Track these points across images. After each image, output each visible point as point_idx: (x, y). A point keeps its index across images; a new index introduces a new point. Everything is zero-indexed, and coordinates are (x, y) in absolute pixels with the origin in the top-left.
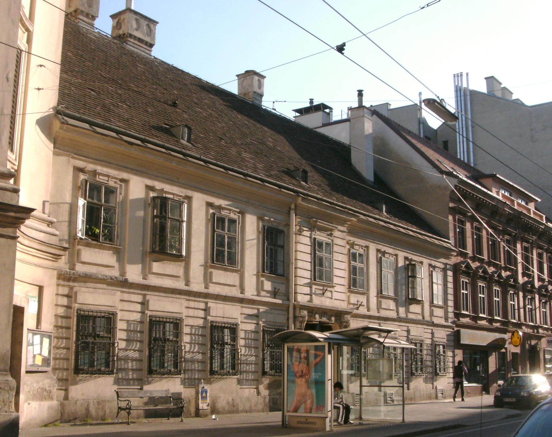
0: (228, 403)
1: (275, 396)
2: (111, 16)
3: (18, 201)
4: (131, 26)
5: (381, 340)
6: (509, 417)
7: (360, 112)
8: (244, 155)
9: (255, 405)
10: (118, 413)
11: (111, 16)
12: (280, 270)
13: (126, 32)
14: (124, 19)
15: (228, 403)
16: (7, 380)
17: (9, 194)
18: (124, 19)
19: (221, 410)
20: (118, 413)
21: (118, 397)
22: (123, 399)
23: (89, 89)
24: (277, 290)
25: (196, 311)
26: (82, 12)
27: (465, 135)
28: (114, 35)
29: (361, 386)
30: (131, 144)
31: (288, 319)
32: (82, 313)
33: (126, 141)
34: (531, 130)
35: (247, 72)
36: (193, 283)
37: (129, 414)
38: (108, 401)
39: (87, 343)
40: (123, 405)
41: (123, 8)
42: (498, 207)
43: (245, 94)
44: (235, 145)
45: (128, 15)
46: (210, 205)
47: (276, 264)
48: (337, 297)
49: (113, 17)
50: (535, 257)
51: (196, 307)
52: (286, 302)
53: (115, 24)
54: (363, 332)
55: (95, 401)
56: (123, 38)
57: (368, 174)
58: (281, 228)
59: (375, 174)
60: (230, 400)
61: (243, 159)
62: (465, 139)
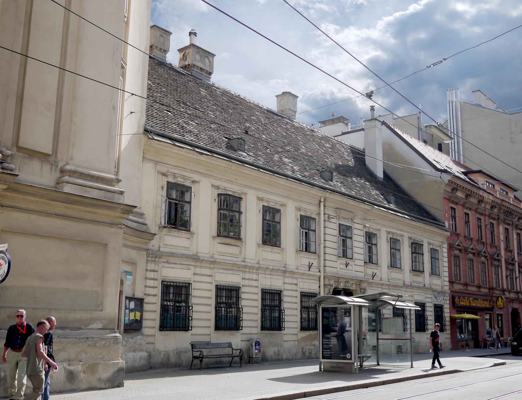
0: (275, 352)
1: (310, 347)
2: (178, 50)
3: (124, 201)
4: (193, 59)
5: (393, 303)
6: (496, 365)
7: (373, 123)
8: (286, 160)
9: (296, 355)
10: (193, 361)
11: (178, 50)
12: (312, 249)
13: (190, 63)
14: (189, 53)
15: (275, 352)
16: (116, 336)
17: (117, 195)
18: (189, 53)
19: (270, 358)
20: (193, 361)
21: (192, 348)
22: (196, 350)
23: (167, 111)
24: (311, 264)
25: (250, 281)
26: (157, 47)
27: (456, 150)
28: (181, 65)
29: (378, 339)
30: (202, 154)
31: (319, 287)
32: (165, 283)
33: (197, 152)
34: (511, 133)
35: (283, 93)
36: (145, 327)
37: (201, 361)
38: (185, 352)
39: (177, 310)
40: (197, 354)
41: (188, 44)
42: (483, 197)
43: (282, 111)
44: (278, 152)
45: (191, 51)
46: (260, 199)
47: (310, 244)
48: (357, 269)
49: (180, 50)
50: (515, 236)
51: (250, 278)
52: (319, 274)
53: (182, 57)
54: (380, 297)
55: (175, 352)
56: (188, 68)
57: (380, 174)
58: (313, 216)
59: (384, 172)
60: (276, 350)
61: (284, 164)
62: (456, 154)
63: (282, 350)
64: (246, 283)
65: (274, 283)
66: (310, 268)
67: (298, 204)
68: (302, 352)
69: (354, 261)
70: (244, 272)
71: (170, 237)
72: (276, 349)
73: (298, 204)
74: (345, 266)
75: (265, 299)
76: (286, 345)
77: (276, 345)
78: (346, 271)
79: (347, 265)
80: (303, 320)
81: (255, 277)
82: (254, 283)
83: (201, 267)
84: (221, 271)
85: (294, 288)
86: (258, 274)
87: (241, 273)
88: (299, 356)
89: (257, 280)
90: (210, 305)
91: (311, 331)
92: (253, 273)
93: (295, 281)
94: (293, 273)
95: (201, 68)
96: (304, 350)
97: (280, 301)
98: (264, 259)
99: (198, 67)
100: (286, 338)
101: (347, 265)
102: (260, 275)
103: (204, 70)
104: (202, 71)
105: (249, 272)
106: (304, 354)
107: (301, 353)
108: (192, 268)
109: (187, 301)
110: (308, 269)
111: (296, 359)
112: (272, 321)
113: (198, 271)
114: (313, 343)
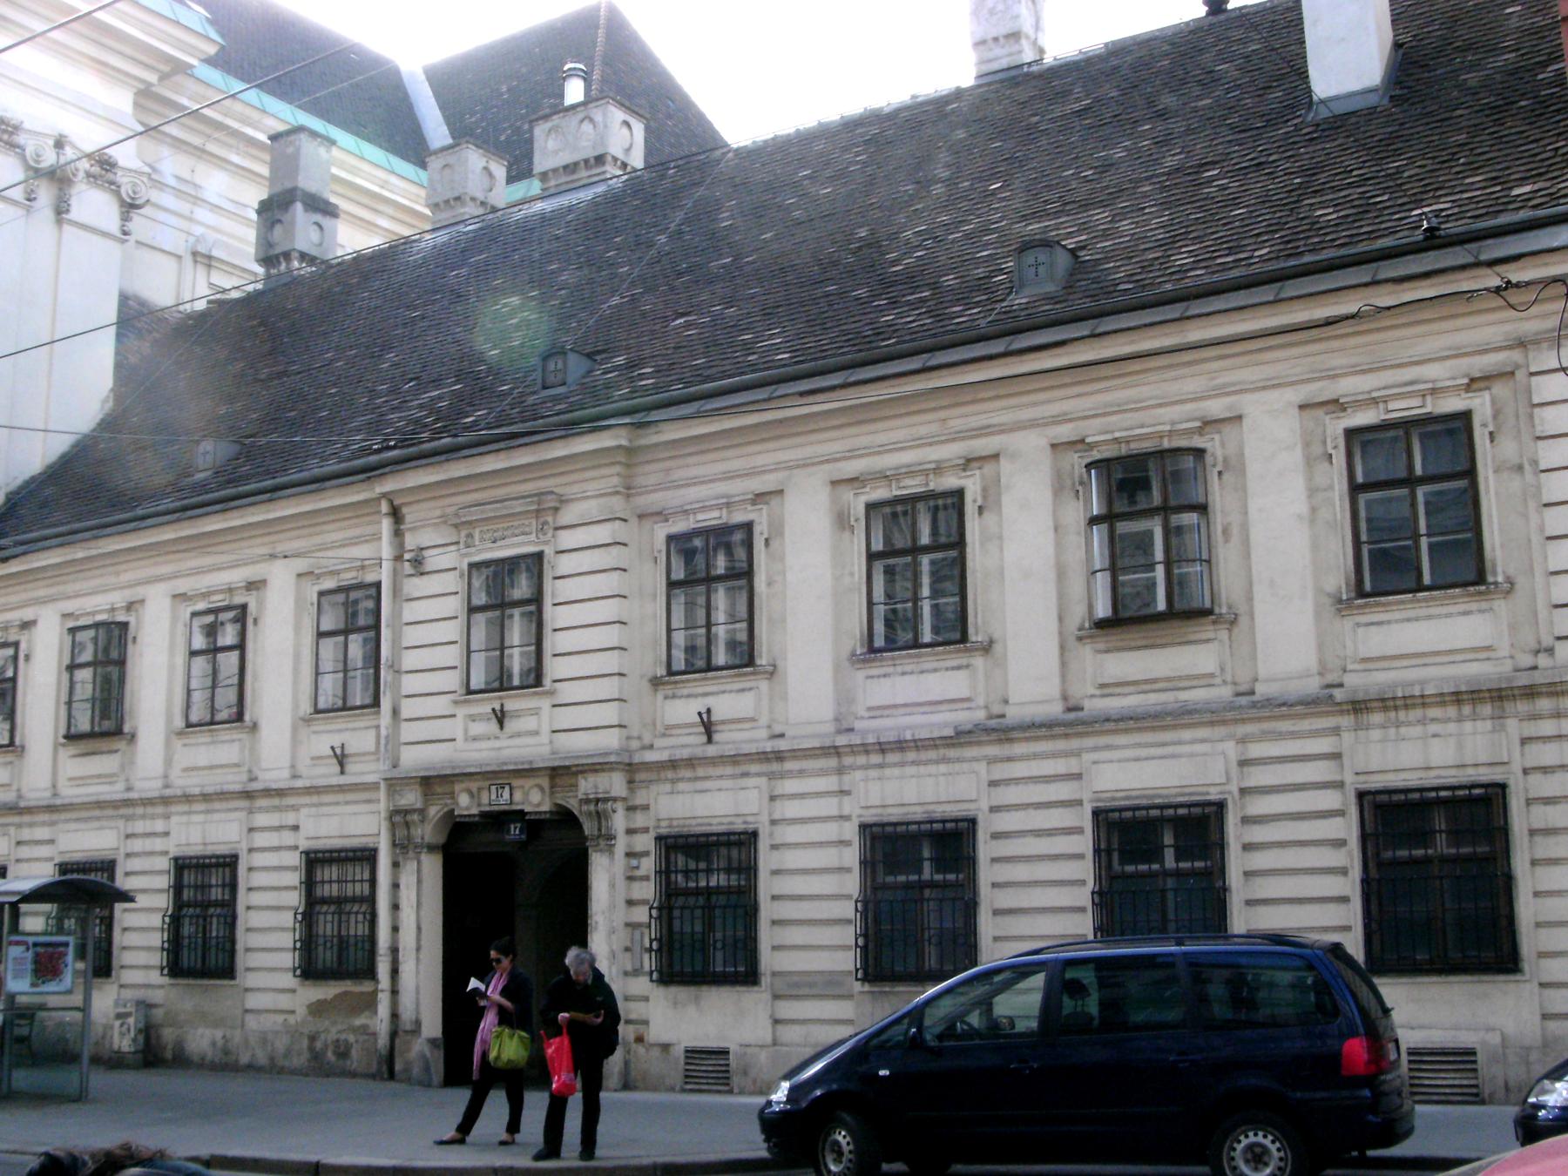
0: (214, 1044)
9: (288, 1053)
15: (214, 1044)
19: (196, 1059)
24: (338, 751)
63: (237, 1036)
64: (137, 845)
65: (210, 833)
66: (341, 764)
67: (301, 565)
68: (311, 1049)
69: (552, 693)
70: (128, 818)
71: (678, 702)
72: (219, 1034)
73: (301, 565)
74: (493, 726)
75: (224, 886)
76: (252, 1023)
77: (218, 1023)
78: (497, 744)
79: (501, 717)
80: (228, 946)
81: (159, 826)
82: (158, 844)
83: (31, 825)
84: (73, 826)
85: (288, 838)
86: (167, 817)
87: (121, 823)
88: (300, 1060)
89: (167, 834)
90: (997, 912)
91: (349, 982)
92: (153, 817)
93: (290, 818)
94: (280, 793)
95: (565, 167)
96: (319, 1045)
97: (233, 886)
98: (1102, 686)
99: (555, 170)
100: (253, 1001)
101: (501, 717)
102: (174, 819)
103: (576, 164)
104: (573, 172)
105: (143, 817)
106: (316, 1056)
107: (306, 1055)
108: (12, 830)
109: (179, 904)
110: (338, 769)
111: (282, 1071)
112: (336, 948)
113: (26, 834)
114: (358, 1022)
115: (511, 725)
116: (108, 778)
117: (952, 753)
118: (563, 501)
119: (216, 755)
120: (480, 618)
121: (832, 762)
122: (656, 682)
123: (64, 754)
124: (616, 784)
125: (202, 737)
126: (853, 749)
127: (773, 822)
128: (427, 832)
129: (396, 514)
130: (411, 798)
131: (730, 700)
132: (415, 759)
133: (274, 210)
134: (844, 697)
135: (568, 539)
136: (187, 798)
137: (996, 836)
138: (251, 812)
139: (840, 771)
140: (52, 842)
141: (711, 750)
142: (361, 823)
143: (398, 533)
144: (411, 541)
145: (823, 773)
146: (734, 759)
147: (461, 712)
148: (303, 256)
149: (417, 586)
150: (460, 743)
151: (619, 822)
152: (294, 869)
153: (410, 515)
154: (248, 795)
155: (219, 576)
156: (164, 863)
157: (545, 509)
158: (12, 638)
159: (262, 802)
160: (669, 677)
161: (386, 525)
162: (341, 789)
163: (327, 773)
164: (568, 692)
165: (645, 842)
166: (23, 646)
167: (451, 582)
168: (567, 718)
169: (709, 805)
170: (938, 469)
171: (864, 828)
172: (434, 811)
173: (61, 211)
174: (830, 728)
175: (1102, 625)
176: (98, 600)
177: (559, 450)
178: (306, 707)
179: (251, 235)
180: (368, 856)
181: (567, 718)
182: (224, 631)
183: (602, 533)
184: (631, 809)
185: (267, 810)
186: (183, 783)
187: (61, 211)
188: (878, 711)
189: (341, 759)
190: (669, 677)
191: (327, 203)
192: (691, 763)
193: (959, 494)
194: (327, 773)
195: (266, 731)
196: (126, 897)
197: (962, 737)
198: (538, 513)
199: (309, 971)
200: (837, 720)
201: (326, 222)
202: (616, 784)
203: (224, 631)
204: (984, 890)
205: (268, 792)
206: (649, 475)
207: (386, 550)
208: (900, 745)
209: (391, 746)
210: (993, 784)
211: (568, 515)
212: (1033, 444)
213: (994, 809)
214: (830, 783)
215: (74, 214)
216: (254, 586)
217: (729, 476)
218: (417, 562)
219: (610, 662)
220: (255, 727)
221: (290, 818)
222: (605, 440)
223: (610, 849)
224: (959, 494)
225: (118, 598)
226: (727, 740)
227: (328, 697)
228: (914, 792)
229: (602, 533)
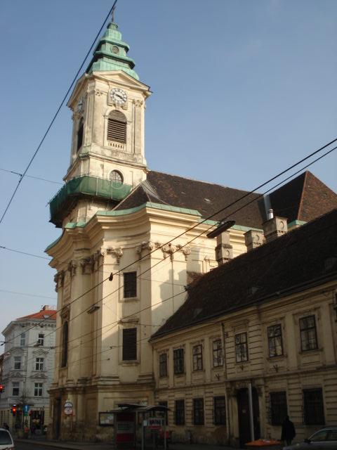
65: (199, 393)
67: (210, 335)
79: (242, 368)
81: (191, 392)
93: (211, 390)
101: (242, 368)
113: (188, 393)
115: (244, 369)
116: (182, 382)
117: (317, 373)
118: (249, 321)
119: (199, 376)
120: (303, 332)
121: (297, 376)
122: (268, 359)
123: (175, 377)
124: (261, 382)
125: (196, 373)
126: (302, 373)
127: (289, 389)
128: (232, 393)
129: (223, 325)
130: (228, 386)
131: (281, 364)
132: (229, 377)
133: (218, 249)
134: (299, 361)
135: (251, 329)
136: (195, 386)
137: (326, 392)
138: (205, 389)
139: (298, 378)
140: (174, 396)
141: (277, 374)
142: (222, 391)
143: (223, 329)
144: (226, 330)
145: (296, 378)
146: (281, 376)
147: (236, 367)
148: (225, 259)
149: (227, 340)
150: (250, 372)
151: (263, 390)
152: (300, 400)
153: (226, 325)
154: (204, 385)
155: (304, 307)
156: (173, 402)
157: (246, 323)
158: (278, 323)
159: (207, 387)
160: (269, 359)
161: (221, 327)
162: (219, 384)
163: (216, 380)
164: (253, 362)
165: (268, 394)
166: (282, 325)
167: (232, 339)
168: (253, 368)
169: (278, 385)
170: (310, 311)
171: (270, 393)
172: (233, 388)
173: (172, 259)
174: (296, 368)
175: (196, 370)
176: (178, 345)
177: (245, 311)
178: (212, 367)
179: (214, 256)
180: (223, 398)
181: (253, 368)
182: (198, 349)
183: (256, 328)
184: (266, 387)
185: (292, 379)
186: (195, 383)
187: (172, 259)
188: (305, 364)
189: (218, 377)
190: (269, 359)
191: (229, 245)
192: (274, 376)
193: (314, 315)
194: (216, 380)
195: (206, 371)
196: (169, 410)
197: (319, 369)
198: (245, 324)
199: (216, 423)
200: (298, 366)
201: (230, 250)
202: (261, 382)
203: (198, 349)
204: (325, 404)
205: (208, 385)
206: (264, 314)
207: (221, 333)
208: (308, 372)
209: (226, 374)
210: (325, 380)
211: (250, 324)
212: (325, 304)
213: (325, 386)
214: (297, 381)
215: (175, 259)
216: (202, 341)
217: (276, 314)
218: (227, 335)
219: (260, 355)
220: (205, 371)
221: (211, 390)
222: (252, 309)
223: (261, 396)
224: (314, 315)
225: (181, 344)
226: (281, 372)
227: (196, 368)
228: (312, 382)
229: (256, 328)
